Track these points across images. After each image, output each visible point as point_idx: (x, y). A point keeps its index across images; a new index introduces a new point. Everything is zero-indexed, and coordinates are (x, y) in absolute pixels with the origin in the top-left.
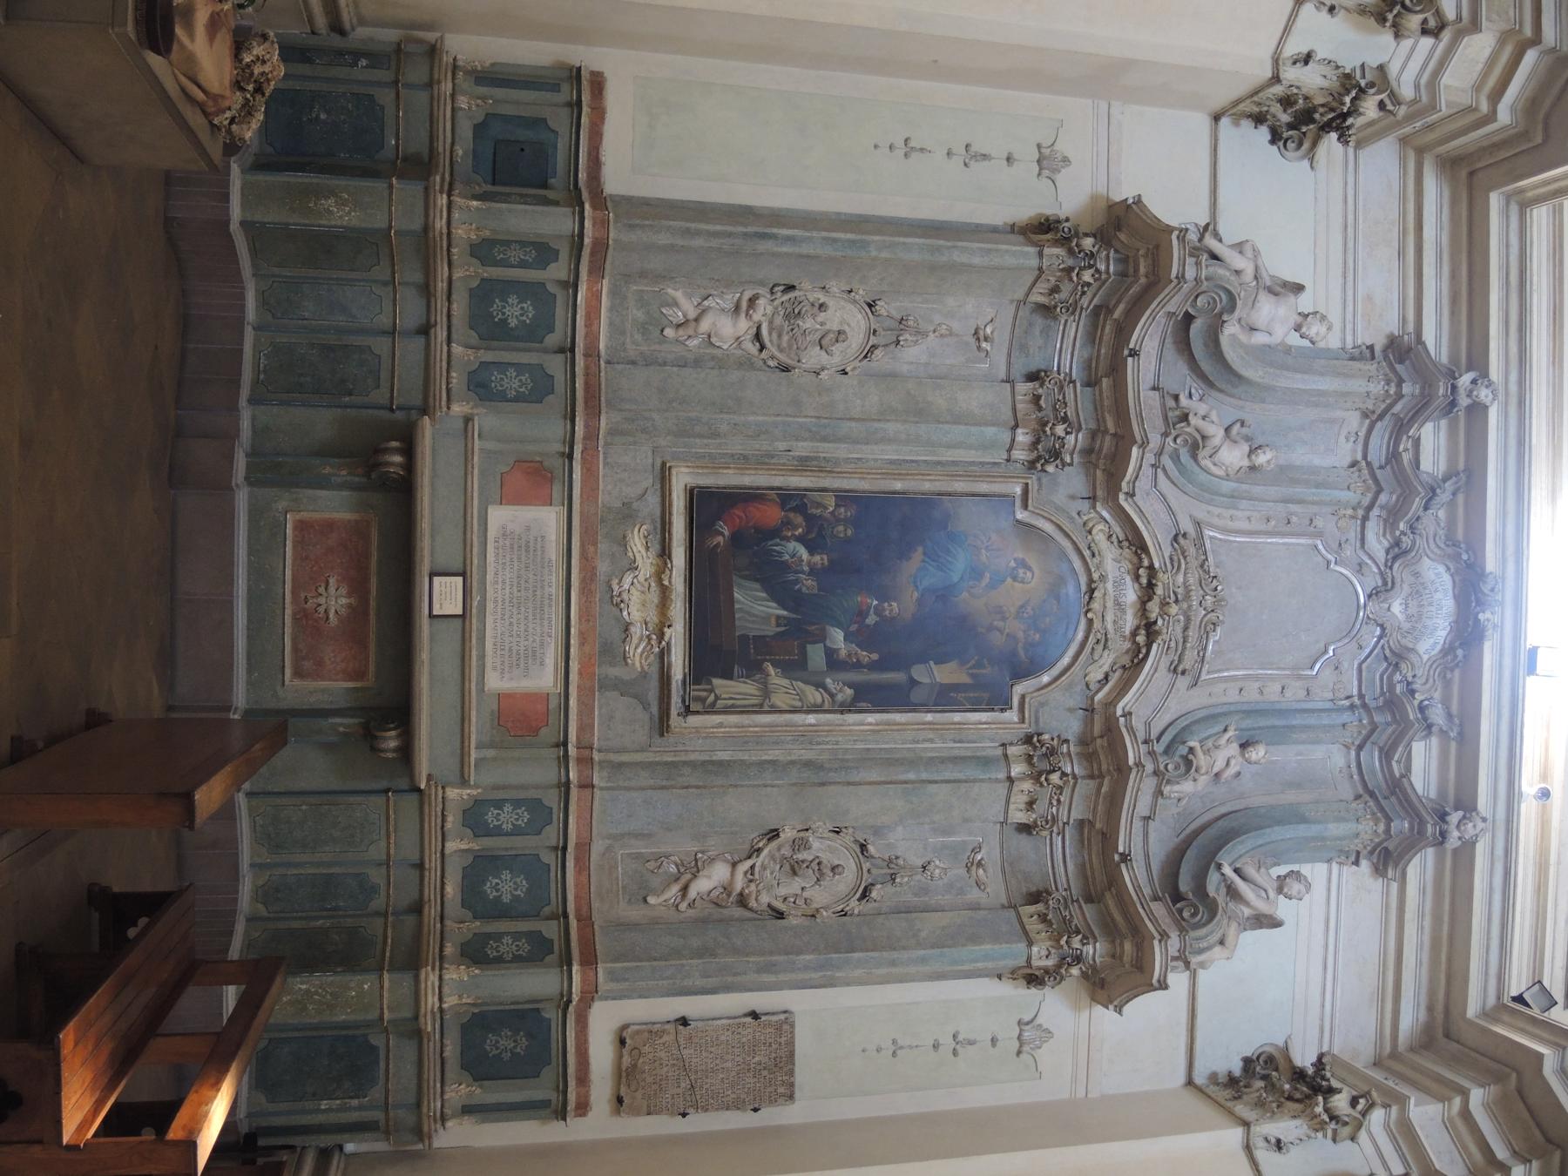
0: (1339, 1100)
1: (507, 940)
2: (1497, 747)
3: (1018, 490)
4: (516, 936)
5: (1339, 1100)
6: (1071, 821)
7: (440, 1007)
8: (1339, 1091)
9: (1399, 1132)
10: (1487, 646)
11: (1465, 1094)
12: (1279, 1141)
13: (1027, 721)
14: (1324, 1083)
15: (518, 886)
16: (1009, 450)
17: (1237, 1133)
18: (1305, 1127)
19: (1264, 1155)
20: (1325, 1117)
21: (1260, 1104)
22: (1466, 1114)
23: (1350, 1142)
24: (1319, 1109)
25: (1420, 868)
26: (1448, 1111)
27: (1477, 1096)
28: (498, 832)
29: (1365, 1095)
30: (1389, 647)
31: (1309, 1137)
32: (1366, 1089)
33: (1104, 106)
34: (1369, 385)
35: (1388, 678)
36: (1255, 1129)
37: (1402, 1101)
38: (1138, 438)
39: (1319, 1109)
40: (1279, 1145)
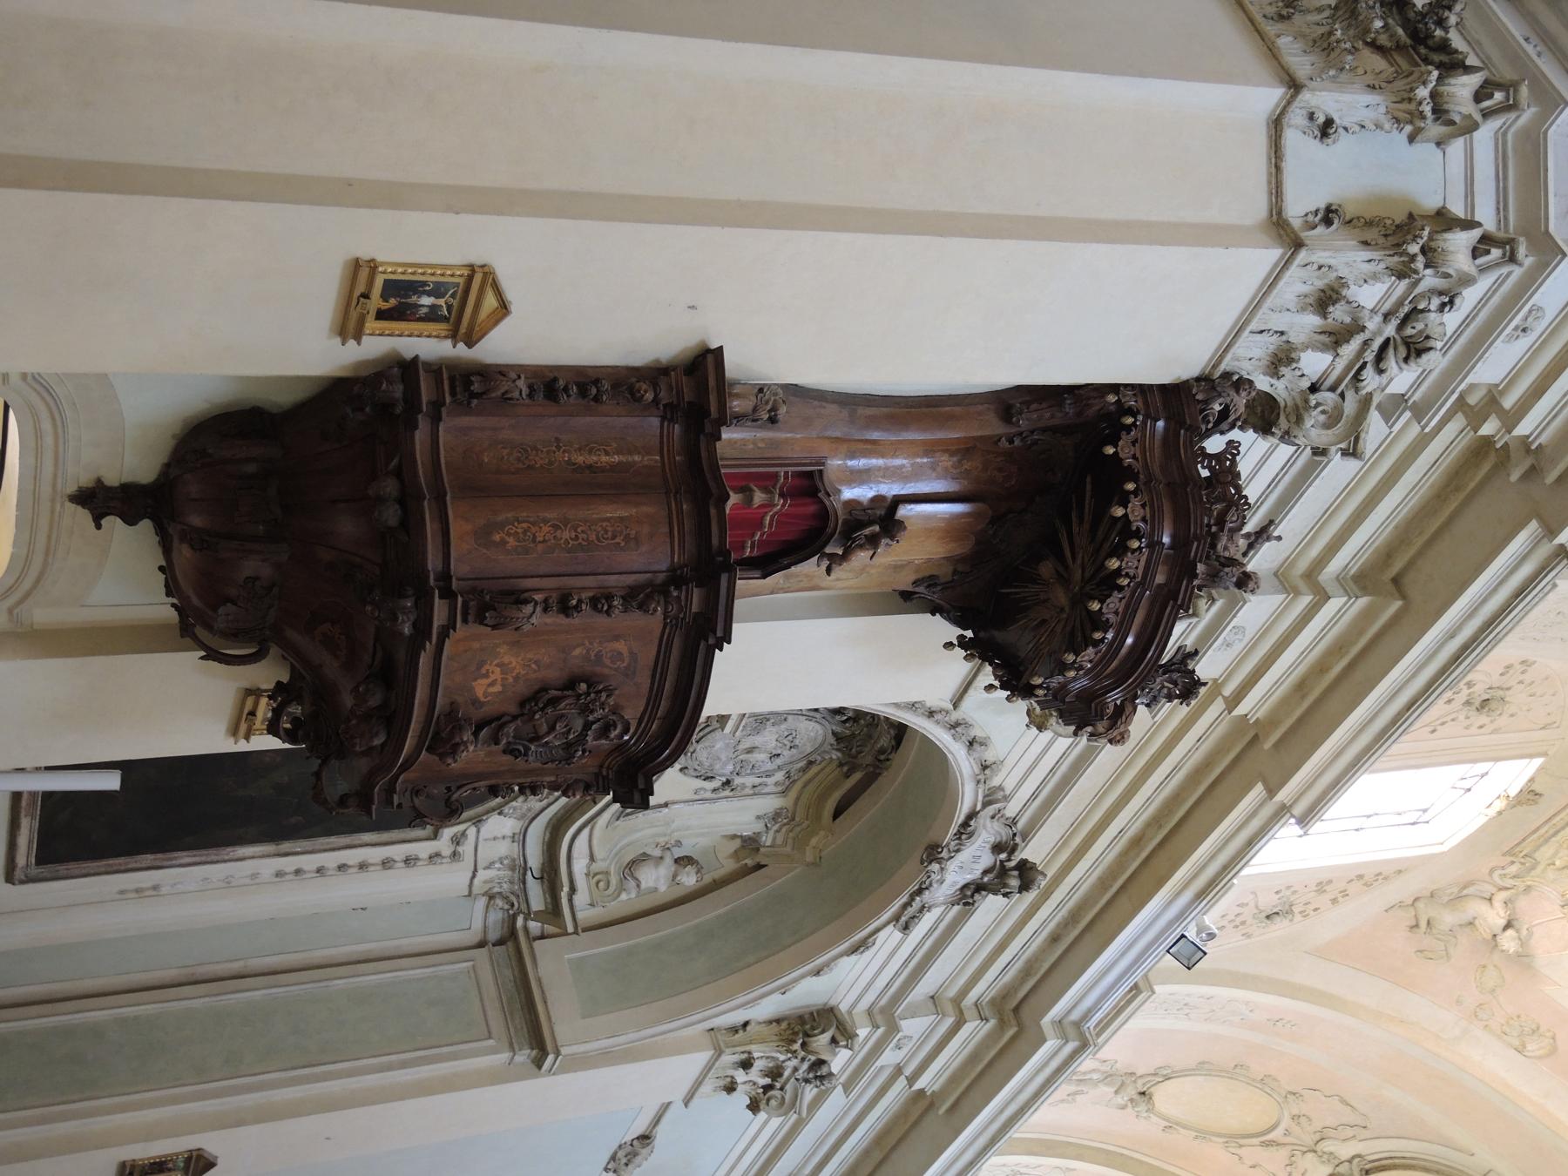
0: (1463, 85)
5: (1463, 85)
8: (1468, 70)
9: (1515, 151)
12: (1329, 122)
14: (1438, 33)
17: (1272, 95)
18: (1382, 109)
19: (1297, 140)
20: (1427, 109)
21: (1324, 46)
23: (1434, 145)
24: (1423, 92)
29: (1509, 87)
31: (1378, 126)
32: (1515, 77)
36: (1307, 98)
38: (714, 491)
39: (1423, 92)
40: (1326, 129)
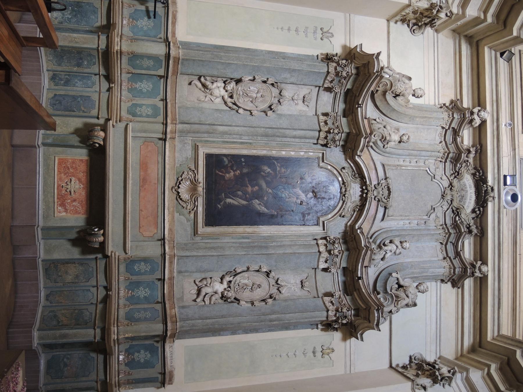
1: (144, 107)
2: (494, 248)
3: (321, 155)
4: (148, 106)
6: (341, 268)
7: (117, 339)
10: (490, 205)
11: (489, 367)
13: (325, 230)
15: (148, 111)
16: (318, 140)
22: (489, 374)
25: (468, 283)
26: (483, 374)
27: (493, 367)
28: (139, 273)
30: (454, 207)
33: (348, 15)
34: (444, 117)
35: (454, 218)
37: (467, 370)
